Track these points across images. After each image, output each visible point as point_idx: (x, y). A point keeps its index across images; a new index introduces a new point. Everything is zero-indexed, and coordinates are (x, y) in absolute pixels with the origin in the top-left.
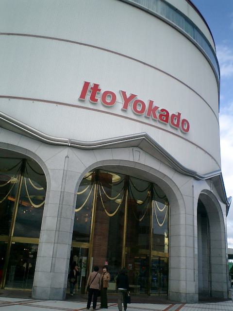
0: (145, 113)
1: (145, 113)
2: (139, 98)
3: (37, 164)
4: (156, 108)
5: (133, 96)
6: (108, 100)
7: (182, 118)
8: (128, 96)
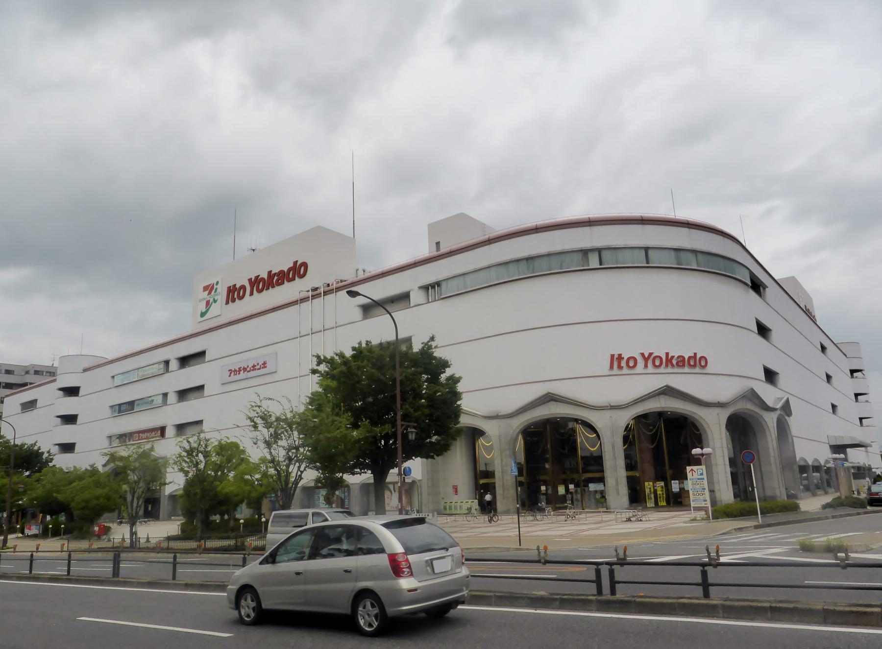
4: (673, 357)
5: (651, 354)
6: (703, 363)
7: (698, 357)
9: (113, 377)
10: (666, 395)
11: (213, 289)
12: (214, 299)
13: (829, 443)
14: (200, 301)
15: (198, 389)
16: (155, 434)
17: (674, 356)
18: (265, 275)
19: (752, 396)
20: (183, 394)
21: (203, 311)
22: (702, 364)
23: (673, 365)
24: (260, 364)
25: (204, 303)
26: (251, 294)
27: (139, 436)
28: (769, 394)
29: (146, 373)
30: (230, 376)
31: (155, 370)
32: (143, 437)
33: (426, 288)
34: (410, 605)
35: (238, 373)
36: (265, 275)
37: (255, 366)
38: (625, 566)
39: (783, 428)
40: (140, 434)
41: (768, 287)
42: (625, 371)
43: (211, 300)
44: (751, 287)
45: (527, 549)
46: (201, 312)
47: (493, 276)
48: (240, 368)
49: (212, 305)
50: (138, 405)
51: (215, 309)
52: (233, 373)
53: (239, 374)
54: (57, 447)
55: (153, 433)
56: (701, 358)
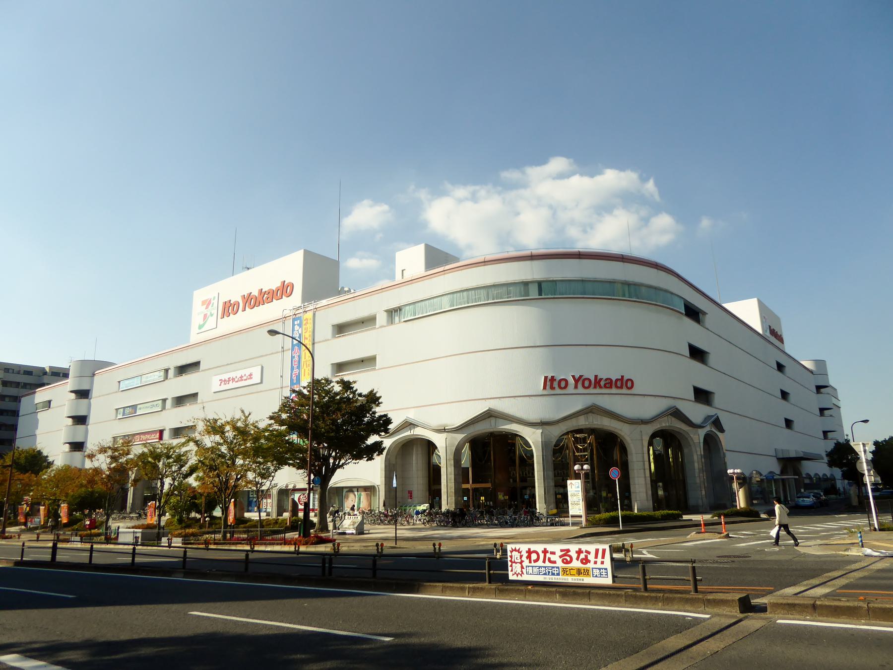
0: (593, 386)
1: (593, 386)
2: (558, 378)
3: (534, 487)
4: (601, 379)
5: (581, 377)
6: (629, 384)
7: (625, 378)
8: (577, 377)
9: (119, 382)
10: (593, 413)
11: (210, 303)
12: (211, 313)
13: (776, 456)
14: (198, 314)
15: (194, 396)
16: (155, 436)
17: (602, 379)
18: (256, 293)
19: (677, 414)
20: (180, 401)
21: (201, 324)
22: (618, 385)
23: (601, 387)
24: (247, 375)
25: (202, 316)
26: (244, 310)
27: (140, 438)
28: (696, 412)
29: (148, 379)
30: (220, 385)
31: (156, 377)
32: (144, 439)
33: (393, 313)
34: (353, 592)
35: (227, 382)
36: (256, 293)
37: (234, 379)
38: (209, 551)
39: (711, 442)
40: (142, 436)
41: (707, 314)
42: (558, 391)
43: (209, 314)
44: (685, 314)
45: (400, 548)
46: (200, 325)
47: (445, 303)
48: (229, 378)
49: (209, 319)
50: (140, 409)
51: (211, 322)
52: (223, 383)
53: (228, 384)
54: (68, 445)
55: (153, 435)
56: (628, 380)
